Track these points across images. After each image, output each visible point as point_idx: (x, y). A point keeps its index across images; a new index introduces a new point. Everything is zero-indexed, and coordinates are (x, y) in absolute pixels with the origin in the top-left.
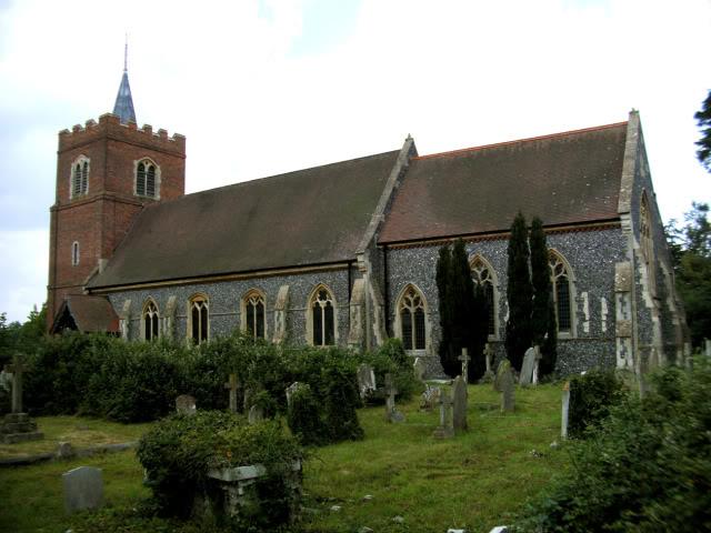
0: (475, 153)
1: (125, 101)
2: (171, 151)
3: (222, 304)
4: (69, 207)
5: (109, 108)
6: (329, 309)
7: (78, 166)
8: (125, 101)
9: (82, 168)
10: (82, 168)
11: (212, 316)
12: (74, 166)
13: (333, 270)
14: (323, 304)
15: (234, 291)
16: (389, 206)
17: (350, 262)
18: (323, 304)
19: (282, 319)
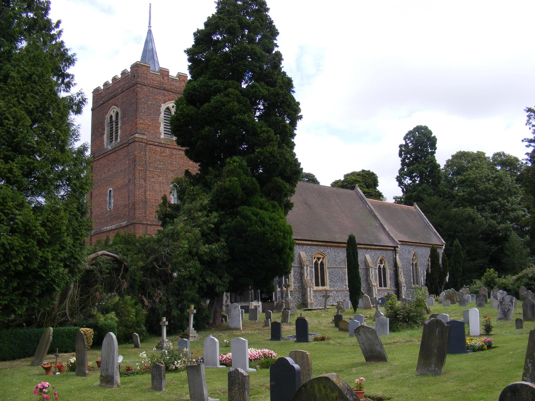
0: (288, 156)
1: (149, 51)
2: (397, 176)
3: (335, 261)
4: (107, 154)
5: (138, 58)
6: (384, 269)
7: (111, 117)
8: (149, 51)
9: (114, 119)
10: (114, 119)
11: (328, 268)
12: (108, 116)
13: (386, 250)
14: (382, 266)
15: (315, 251)
16: (371, 212)
17: (395, 247)
18: (382, 266)
19: (373, 273)
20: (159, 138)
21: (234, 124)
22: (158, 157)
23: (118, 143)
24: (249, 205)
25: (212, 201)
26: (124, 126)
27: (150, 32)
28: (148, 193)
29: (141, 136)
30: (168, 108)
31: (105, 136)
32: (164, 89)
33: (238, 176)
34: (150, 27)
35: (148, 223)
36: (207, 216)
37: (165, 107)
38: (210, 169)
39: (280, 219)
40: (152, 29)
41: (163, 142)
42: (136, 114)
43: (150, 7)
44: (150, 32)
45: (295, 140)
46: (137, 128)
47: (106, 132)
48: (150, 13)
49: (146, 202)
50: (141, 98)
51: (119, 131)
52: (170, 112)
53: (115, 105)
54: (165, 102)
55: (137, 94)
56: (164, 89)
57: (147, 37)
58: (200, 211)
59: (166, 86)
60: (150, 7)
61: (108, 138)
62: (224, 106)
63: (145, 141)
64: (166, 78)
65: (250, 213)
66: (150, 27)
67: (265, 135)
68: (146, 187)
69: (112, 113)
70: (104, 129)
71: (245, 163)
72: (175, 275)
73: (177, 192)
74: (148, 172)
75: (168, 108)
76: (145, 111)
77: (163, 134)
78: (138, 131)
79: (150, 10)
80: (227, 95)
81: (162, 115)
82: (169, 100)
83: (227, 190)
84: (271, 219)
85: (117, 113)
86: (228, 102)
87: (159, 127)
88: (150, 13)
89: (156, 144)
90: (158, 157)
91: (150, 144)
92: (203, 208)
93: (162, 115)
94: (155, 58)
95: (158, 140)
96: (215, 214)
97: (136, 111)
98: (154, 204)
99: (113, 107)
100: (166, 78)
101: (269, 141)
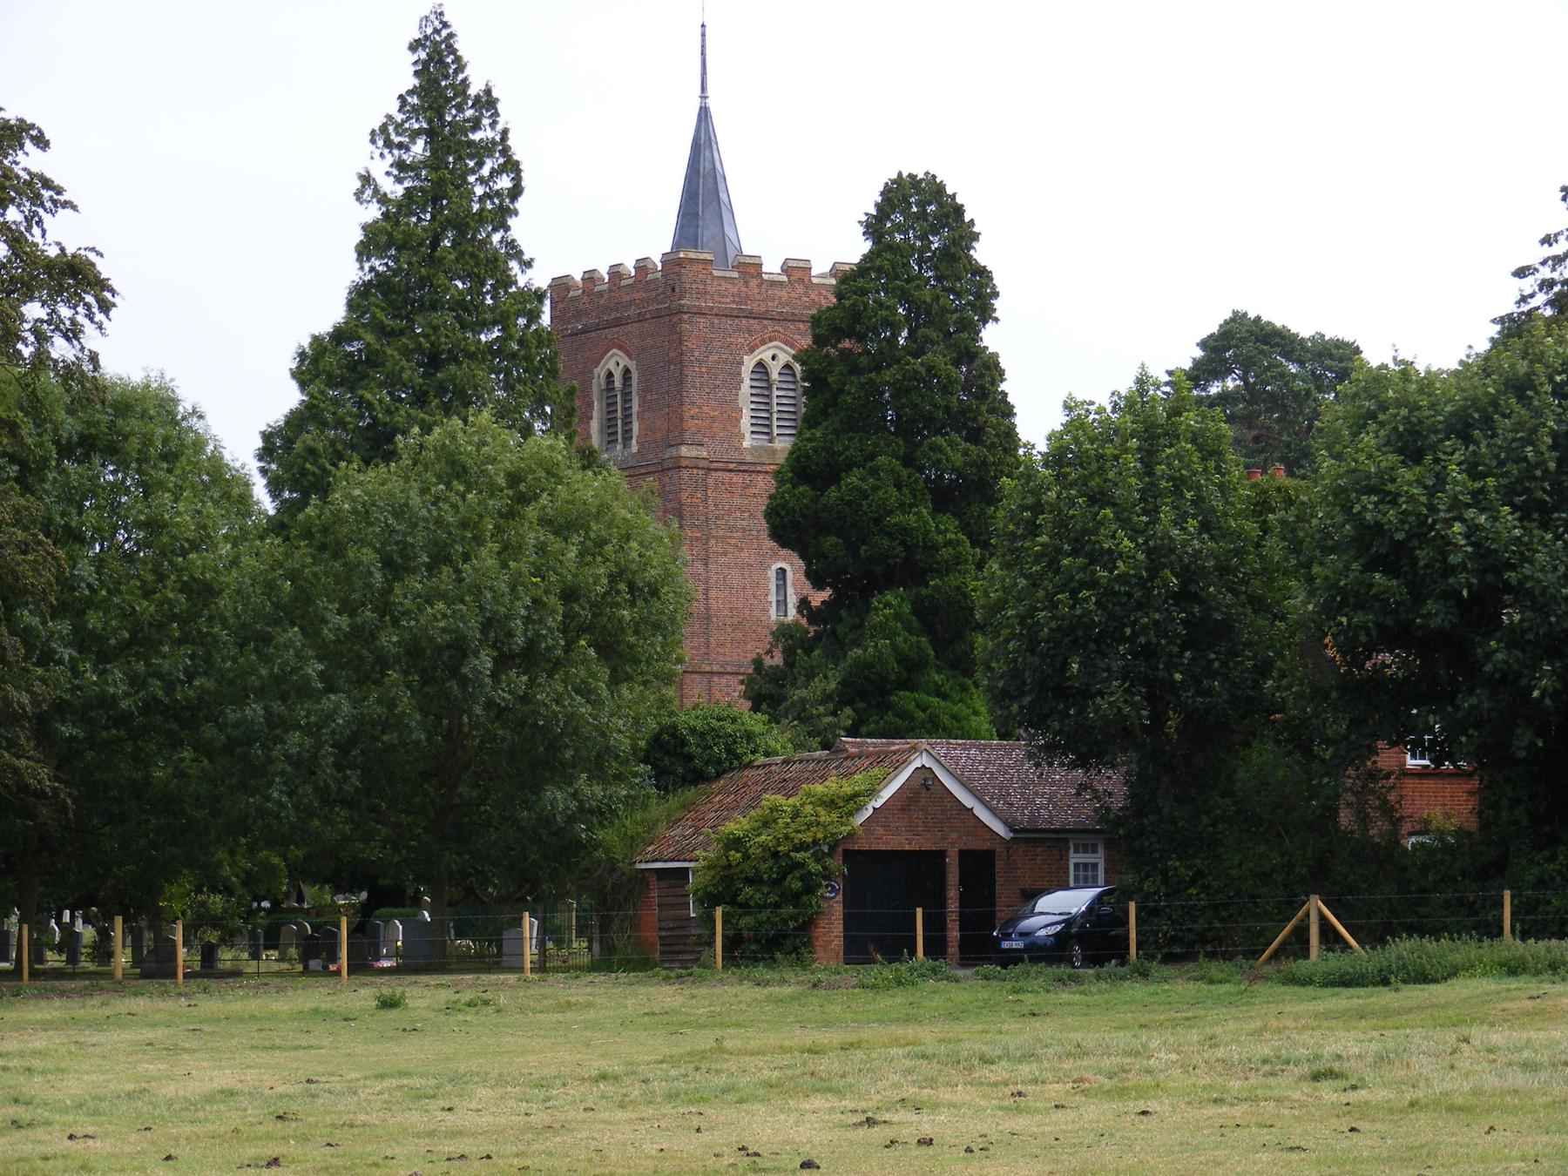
1: (703, 193)
7: (610, 375)
9: (618, 383)
10: (618, 383)
12: (600, 372)
20: (738, 449)
21: (889, 535)
22: (737, 501)
23: (634, 455)
24: (913, 689)
25: (844, 683)
26: (647, 415)
27: (704, 114)
28: (713, 594)
29: (694, 453)
30: (760, 364)
31: (595, 426)
32: (751, 316)
33: (891, 635)
34: (704, 97)
35: (715, 668)
36: (834, 714)
37: (753, 363)
38: (843, 613)
39: (974, 718)
40: (711, 103)
41: (749, 458)
42: (680, 392)
43: (703, 35)
44: (704, 114)
45: (1214, 329)
46: (682, 432)
47: (595, 414)
48: (703, 53)
49: (708, 618)
50: (692, 351)
51: (636, 426)
52: (767, 373)
53: (620, 347)
54: (752, 350)
55: (681, 342)
56: (751, 316)
57: (698, 131)
58: (822, 702)
59: (755, 305)
60: (703, 35)
61: (601, 431)
62: (866, 497)
63: (705, 464)
64: (754, 282)
65: (912, 707)
66: (704, 97)
67: (946, 553)
68: (708, 579)
69: (611, 366)
70: (590, 405)
71: (906, 608)
72: (1178, 677)
73: (783, 652)
74: (713, 542)
75: (760, 364)
76: (702, 384)
77: (747, 435)
78: (687, 436)
79: (703, 46)
80: (874, 472)
81: (747, 383)
82: (763, 342)
83: (870, 666)
84: (954, 717)
85: (627, 371)
86: (875, 489)
87: (738, 421)
88: (703, 53)
89: (731, 466)
90: (737, 501)
91: (716, 470)
92: (827, 698)
93: (747, 383)
94: (723, 196)
95: (736, 456)
96: (848, 711)
97: (681, 383)
98: (729, 621)
99: (614, 351)
100: (754, 282)
101: (959, 564)
